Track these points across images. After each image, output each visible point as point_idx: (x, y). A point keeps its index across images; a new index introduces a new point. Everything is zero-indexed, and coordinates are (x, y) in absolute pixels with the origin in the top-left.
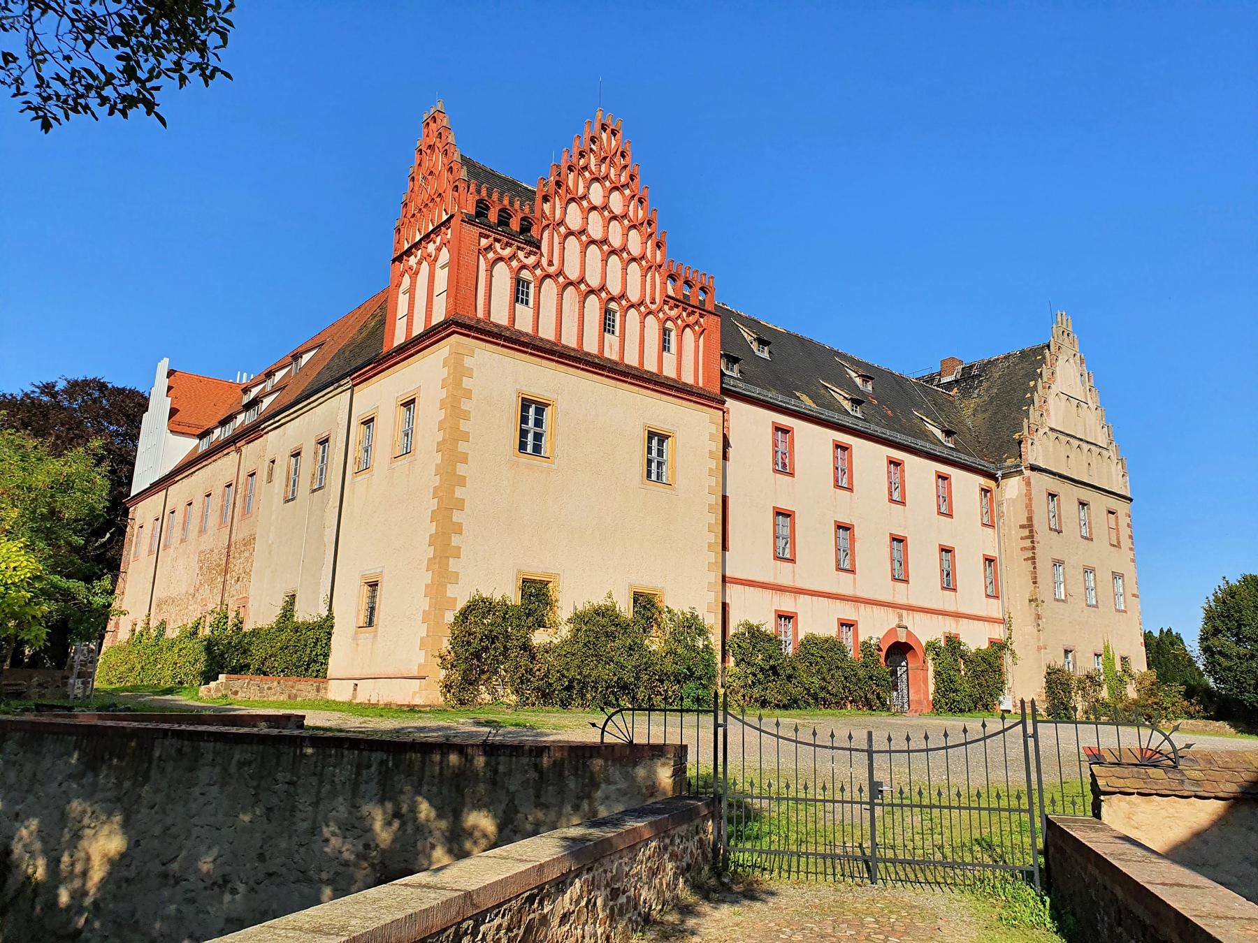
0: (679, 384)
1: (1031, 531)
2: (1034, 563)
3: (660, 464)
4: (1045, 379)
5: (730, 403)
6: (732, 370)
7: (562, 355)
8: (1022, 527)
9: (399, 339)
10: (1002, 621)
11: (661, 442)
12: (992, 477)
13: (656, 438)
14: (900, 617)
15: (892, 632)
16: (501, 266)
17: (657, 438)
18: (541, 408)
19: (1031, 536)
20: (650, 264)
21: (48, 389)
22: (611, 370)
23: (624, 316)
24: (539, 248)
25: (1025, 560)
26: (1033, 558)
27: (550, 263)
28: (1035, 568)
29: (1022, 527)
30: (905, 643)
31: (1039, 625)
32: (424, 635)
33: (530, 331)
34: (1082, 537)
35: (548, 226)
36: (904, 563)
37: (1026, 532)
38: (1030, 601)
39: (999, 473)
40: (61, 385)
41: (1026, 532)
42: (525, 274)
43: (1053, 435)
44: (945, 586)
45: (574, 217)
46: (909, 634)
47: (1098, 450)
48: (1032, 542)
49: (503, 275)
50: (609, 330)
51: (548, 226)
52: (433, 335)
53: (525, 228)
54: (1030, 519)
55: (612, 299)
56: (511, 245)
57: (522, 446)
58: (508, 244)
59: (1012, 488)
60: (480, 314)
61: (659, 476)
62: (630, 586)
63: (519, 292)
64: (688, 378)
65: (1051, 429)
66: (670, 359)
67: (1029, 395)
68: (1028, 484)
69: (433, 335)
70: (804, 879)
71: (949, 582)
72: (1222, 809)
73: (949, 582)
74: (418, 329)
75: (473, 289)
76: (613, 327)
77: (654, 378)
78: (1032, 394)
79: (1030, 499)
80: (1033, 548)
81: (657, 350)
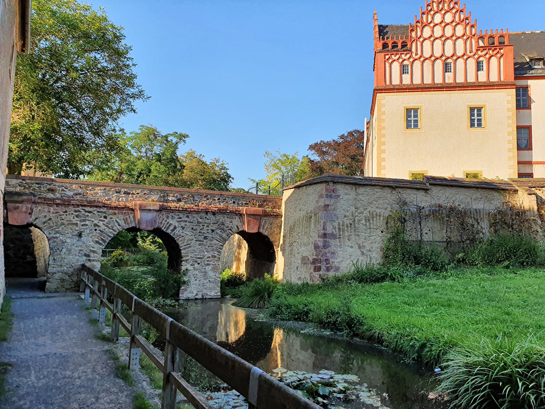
6: (539, 65)
13: (476, 109)
16: (395, 63)
18: (479, 109)
20: (468, 37)
21: (342, 137)
22: (484, 86)
23: (455, 63)
27: (416, 54)
35: (414, 40)
40: (346, 135)
42: (406, 63)
45: (427, 32)
49: (396, 66)
50: (406, 72)
51: (414, 40)
53: (404, 45)
55: (448, 58)
56: (398, 54)
57: (472, 125)
58: (407, 54)
60: (388, 83)
62: (464, 171)
63: (403, 70)
70: (74, 234)
75: (384, 75)
76: (451, 69)
81: (474, 72)
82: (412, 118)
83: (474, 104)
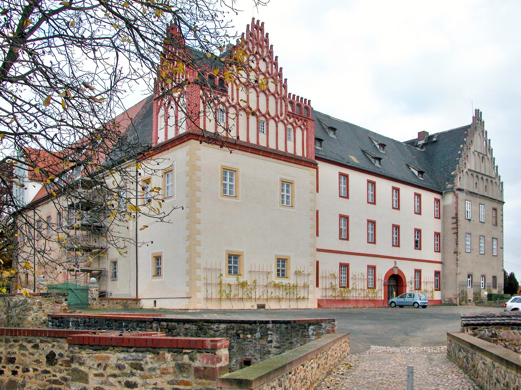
0: (295, 156)
1: (457, 220)
2: (457, 235)
3: (288, 197)
4: (468, 145)
5: (321, 165)
7: (295, 159)
8: (453, 218)
9: (161, 140)
10: (441, 263)
11: (288, 186)
12: (441, 194)
14: (395, 262)
15: (392, 270)
17: (286, 184)
19: (457, 223)
24: (227, 92)
25: (453, 234)
26: (457, 233)
27: (233, 100)
28: (457, 237)
29: (453, 218)
30: (397, 275)
31: (457, 264)
32: (188, 280)
33: (275, 148)
34: (480, 222)
36: (398, 239)
37: (454, 221)
38: (454, 253)
39: (444, 192)
41: (454, 221)
43: (470, 173)
44: (436, 250)
46: (399, 271)
47: (476, 174)
48: (457, 225)
52: (179, 140)
54: (457, 214)
59: (449, 199)
61: (231, 192)
64: (299, 153)
65: (469, 170)
66: (95, 91)
67: (460, 152)
68: (457, 197)
69: (179, 140)
71: (418, 245)
72: (227, 384)
73: (418, 245)
74: (171, 135)
77: (245, 145)
78: (461, 152)
79: (457, 205)
80: (457, 228)
82: (228, 182)
83: (229, 165)
